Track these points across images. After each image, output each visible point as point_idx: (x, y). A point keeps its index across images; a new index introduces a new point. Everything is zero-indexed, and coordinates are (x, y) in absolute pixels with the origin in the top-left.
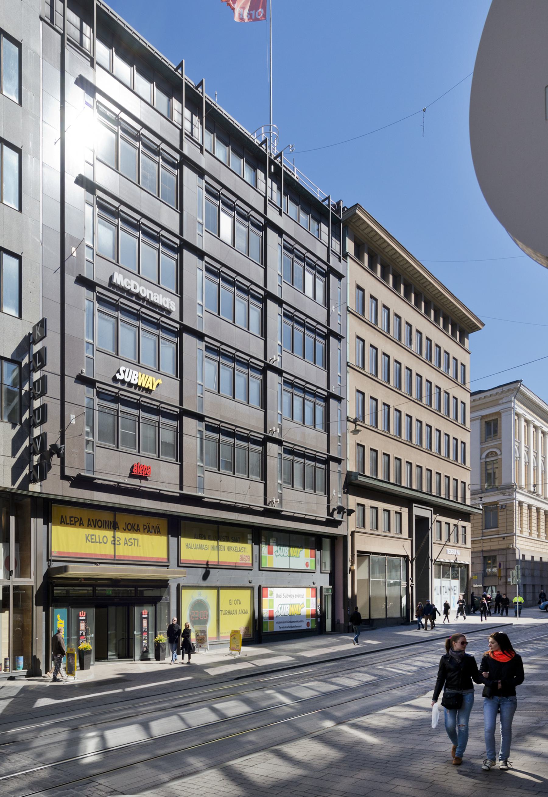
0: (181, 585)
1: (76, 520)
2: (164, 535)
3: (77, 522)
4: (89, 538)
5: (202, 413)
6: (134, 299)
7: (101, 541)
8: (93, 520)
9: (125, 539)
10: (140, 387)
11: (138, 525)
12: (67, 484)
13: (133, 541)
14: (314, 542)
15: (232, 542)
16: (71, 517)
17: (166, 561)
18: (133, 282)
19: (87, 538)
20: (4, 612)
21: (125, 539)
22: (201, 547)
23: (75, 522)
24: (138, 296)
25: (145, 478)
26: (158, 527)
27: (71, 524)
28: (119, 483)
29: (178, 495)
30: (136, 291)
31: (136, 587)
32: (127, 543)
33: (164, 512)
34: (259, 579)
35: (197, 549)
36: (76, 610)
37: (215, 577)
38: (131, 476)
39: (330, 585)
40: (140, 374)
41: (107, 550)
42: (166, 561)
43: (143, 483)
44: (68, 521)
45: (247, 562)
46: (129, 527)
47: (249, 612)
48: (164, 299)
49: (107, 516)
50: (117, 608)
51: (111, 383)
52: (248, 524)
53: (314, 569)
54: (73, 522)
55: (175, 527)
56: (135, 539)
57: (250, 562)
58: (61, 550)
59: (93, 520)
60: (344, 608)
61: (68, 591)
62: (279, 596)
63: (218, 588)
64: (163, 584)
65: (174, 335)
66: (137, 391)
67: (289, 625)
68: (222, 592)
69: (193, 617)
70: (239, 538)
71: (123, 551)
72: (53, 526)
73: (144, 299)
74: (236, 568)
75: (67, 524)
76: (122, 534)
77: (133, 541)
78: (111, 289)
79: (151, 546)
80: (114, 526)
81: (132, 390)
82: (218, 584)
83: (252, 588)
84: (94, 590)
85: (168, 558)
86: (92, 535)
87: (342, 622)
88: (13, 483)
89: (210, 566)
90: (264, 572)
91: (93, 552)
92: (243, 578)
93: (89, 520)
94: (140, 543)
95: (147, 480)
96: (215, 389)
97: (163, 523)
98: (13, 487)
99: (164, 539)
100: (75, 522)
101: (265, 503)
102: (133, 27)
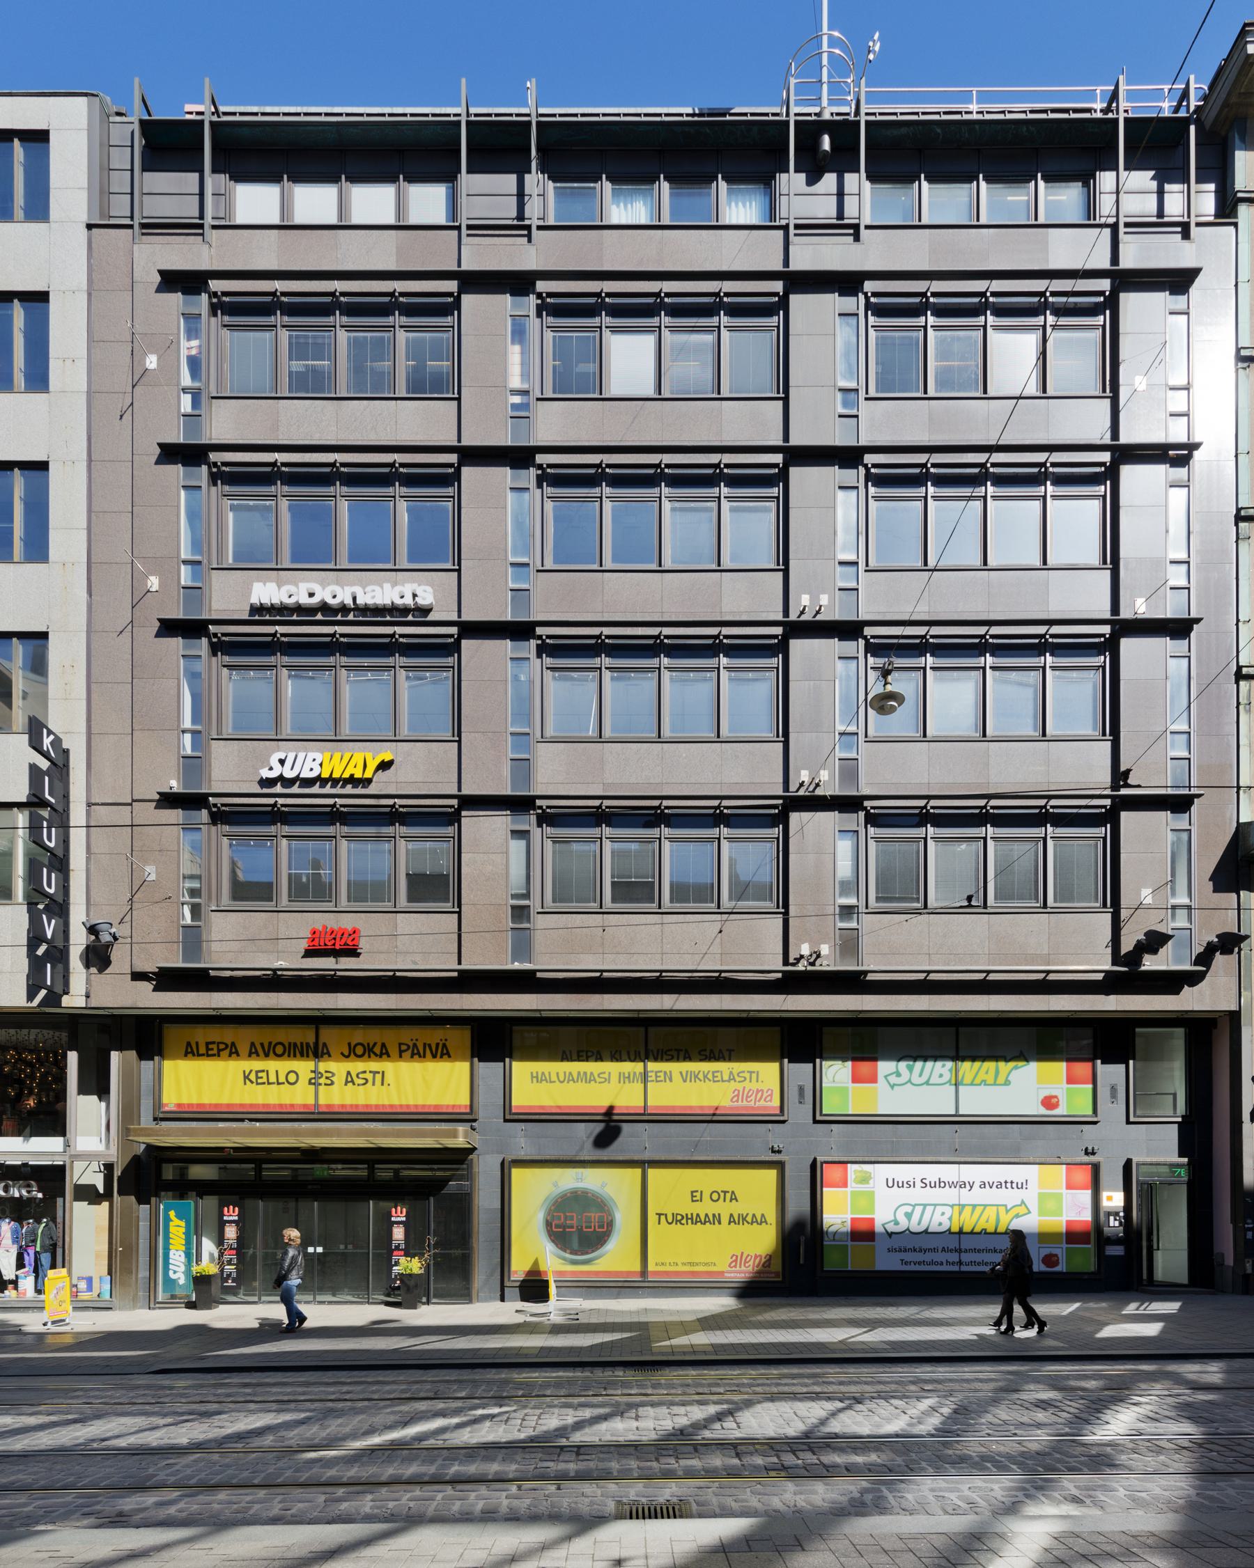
0: (819, 1159)
1: (222, 1046)
2: (463, 1059)
3: (212, 1051)
4: (253, 1077)
5: (855, 793)
6: (319, 617)
7: (282, 1079)
8: (262, 1045)
9: (349, 1073)
10: (335, 782)
11: (383, 1045)
12: (147, 986)
13: (369, 1076)
14: (1108, 1041)
15: (701, 1060)
16: (207, 1044)
17: (468, 1110)
18: (408, 589)
19: (246, 1077)
20: (100, 1204)
21: (349, 1073)
22: (588, 1078)
23: (219, 1051)
24: (324, 607)
25: (353, 952)
26: (444, 1045)
27: (208, 1056)
28: (274, 970)
29: (455, 974)
30: (315, 600)
31: (371, 1165)
32: (352, 1081)
33: (427, 1014)
34: (799, 1143)
35: (538, 1083)
36: (384, 1204)
37: (632, 1139)
38: (309, 953)
39: (1180, 1156)
40: (328, 755)
41: (300, 1096)
42: (778, 1112)
43: (346, 963)
44: (203, 1050)
45: (769, 1104)
46: (359, 1050)
47: (772, 1217)
48: (398, 589)
49: (306, 1035)
50: (415, 1199)
51: (258, 790)
52: (995, 1015)
53: (1090, 1112)
54: (215, 1051)
55: (493, 1041)
56: (751, 1073)
57: (776, 1102)
58: (185, 1101)
59: (262, 1045)
60: (1234, 1220)
61: (396, 1171)
62: (891, 1184)
63: (644, 1164)
64: (460, 1157)
65: (1036, 652)
66: (328, 790)
67: (954, 1257)
68: (652, 1173)
69: (557, 1226)
70: (730, 1051)
71: (337, 1095)
72: (514, 1064)
73: (344, 609)
74: (715, 1118)
75: (199, 1055)
76: (340, 1064)
77: (369, 1076)
78: (257, 618)
79: (440, 1082)
80: (317, 1052)
81: (316, 789)
82: (646, 1156)
83: (780, 1166)
84: (259, 1170)
85: (471, 1106)
86: (257, 1072)
87: (1230, 1261)
88: (31, 997)
89: (615, 1118)
90: (834, 1126)
91: (261, 1102)
92: (759, 1140)
93: (253, 1044)
94: (388, 1078)
95: (358, 955)
96: (1094, 729)
97: (461, 1037)
98: (30, 1005)
99: (465, 1066)
100: (219, 1051)
101: (786, 962)
102: (231, 105)
